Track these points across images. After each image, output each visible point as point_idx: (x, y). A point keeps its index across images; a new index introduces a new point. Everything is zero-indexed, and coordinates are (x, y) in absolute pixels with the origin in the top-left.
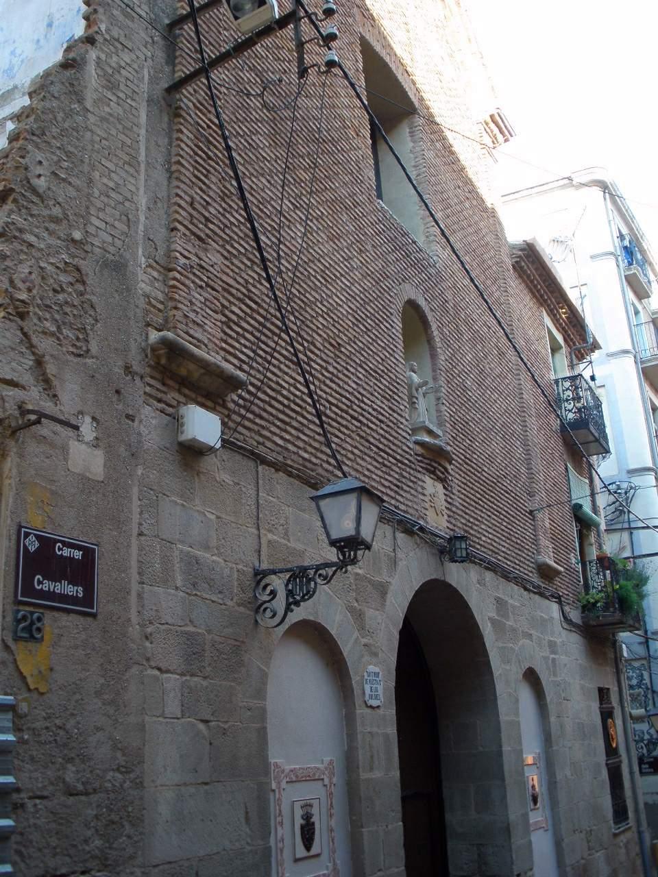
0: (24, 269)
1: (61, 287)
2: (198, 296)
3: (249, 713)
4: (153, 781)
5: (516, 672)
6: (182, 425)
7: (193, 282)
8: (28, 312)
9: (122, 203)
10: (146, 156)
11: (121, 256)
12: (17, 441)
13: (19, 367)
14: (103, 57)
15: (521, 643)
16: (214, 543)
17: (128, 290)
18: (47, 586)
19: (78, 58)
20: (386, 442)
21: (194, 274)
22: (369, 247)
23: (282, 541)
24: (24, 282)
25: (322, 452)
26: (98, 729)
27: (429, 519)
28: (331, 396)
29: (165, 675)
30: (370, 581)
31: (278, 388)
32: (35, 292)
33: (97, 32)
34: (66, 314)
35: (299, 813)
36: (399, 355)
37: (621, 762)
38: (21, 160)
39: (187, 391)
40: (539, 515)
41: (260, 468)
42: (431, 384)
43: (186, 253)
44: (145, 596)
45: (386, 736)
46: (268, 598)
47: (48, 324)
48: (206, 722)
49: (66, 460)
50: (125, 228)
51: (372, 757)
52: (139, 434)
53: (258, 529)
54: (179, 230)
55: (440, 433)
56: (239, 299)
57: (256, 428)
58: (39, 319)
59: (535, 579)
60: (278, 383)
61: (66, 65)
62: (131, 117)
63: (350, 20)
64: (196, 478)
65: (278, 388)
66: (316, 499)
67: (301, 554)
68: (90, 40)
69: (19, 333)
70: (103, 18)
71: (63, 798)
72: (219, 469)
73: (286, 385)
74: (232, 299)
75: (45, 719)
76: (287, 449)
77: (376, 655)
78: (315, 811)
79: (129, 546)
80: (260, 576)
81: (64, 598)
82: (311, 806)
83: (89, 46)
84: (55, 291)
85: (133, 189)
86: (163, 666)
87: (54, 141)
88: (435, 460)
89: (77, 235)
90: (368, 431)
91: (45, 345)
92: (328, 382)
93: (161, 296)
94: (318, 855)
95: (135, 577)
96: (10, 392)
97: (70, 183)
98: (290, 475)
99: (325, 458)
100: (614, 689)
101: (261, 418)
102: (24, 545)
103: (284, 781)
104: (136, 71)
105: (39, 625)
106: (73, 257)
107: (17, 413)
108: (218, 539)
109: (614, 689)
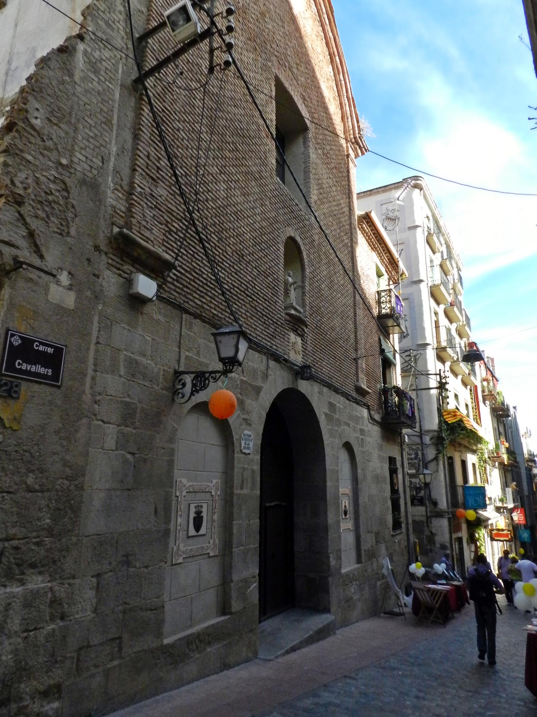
0: (22, 176)
1: (51, 191)
2: (149, 213)
3: (163, 451)
4: (91, 486)
5: (338, 442)
6: (132, 284)
7: (146, 204)
8: (24, 203)
9: (99, 148)
10: (118, 121)
11: (96, 180)
12: (10, 279)
13: (18, 236)
14: (89, 50)
15: (342, 428)
16: (149, 353)
17: (100, 201)
18: (24, 367)
19: (70, 47)
20: (267, 311)
21: (147, 199)
22: (268, 203)
23: (196, 357)
24: (21, 183)
25: (226, 312)
26: (55, 454)
27: (291, 356)
28: (235, 282)
29: (106, 425)
30: (250, 384)
31: (201, 273)
32: (30, 191)
33: (85, 32)
34: (53, 208)
35: (193, 510)
36: (281, 266)
37: (399, 498)
38: (23, 106)
39: (137, 266)
40: (359, 361)
41: (184, 315)
42: (300, 284)
43: (142, 185)
44: (98, 378)
45: (253, 471)
46: (180, 387)
47: (39, 212)
48: (133, 454)
49: (46, 294)
50: (101, 164)
51: (243, 481)
52: (101, 286)
53: (179, 348)
54: (137, 171)
55: (302, 311)
56: (178, 219)
57: (183, 293)
58: (33, 208)
59: (354, 394)
60: (200, 270)
61: (61, 50)
62: (108, 93)
63: (270, 64)
64: (140, 317)
65: (201, 273)
66: (214, 335)
67: (207, 365)
68: (80, 37)
69: (17, 214)
70: (91, 24)
71: (23, 494)
72: (154, 311)
73: (206, 273)
74: (173, 218)
75: (15, 445)
76: (203, 308)
77: (250, 425)
78: (204, 510)
79: (88, 349)
80: (178, 374)
81: (36, 375)
82: (202, 507)
83: (79, 41)
84: (46, 193)
85: (107, 140)
86: (105, 419)
87: (49, 98)
88: (297, 324)
89: (64, 161)
90: (257, 304)
91: (34, 224)
92: (233, 274)
93: (123, 209)
94: (204, 535)
95: (91, 367)
96: (7, 250)
97: (60, 127)
98: (204, 321)
99: (227, 315)
100: (398, 459)
101: (188, 288)
102: (10, 341)
103: (185, 492)
104: (113, 65)
105: (16, 389)
106: (61, 174)
107: (11, 262)
108: (152, 352)
109: (398, 459)
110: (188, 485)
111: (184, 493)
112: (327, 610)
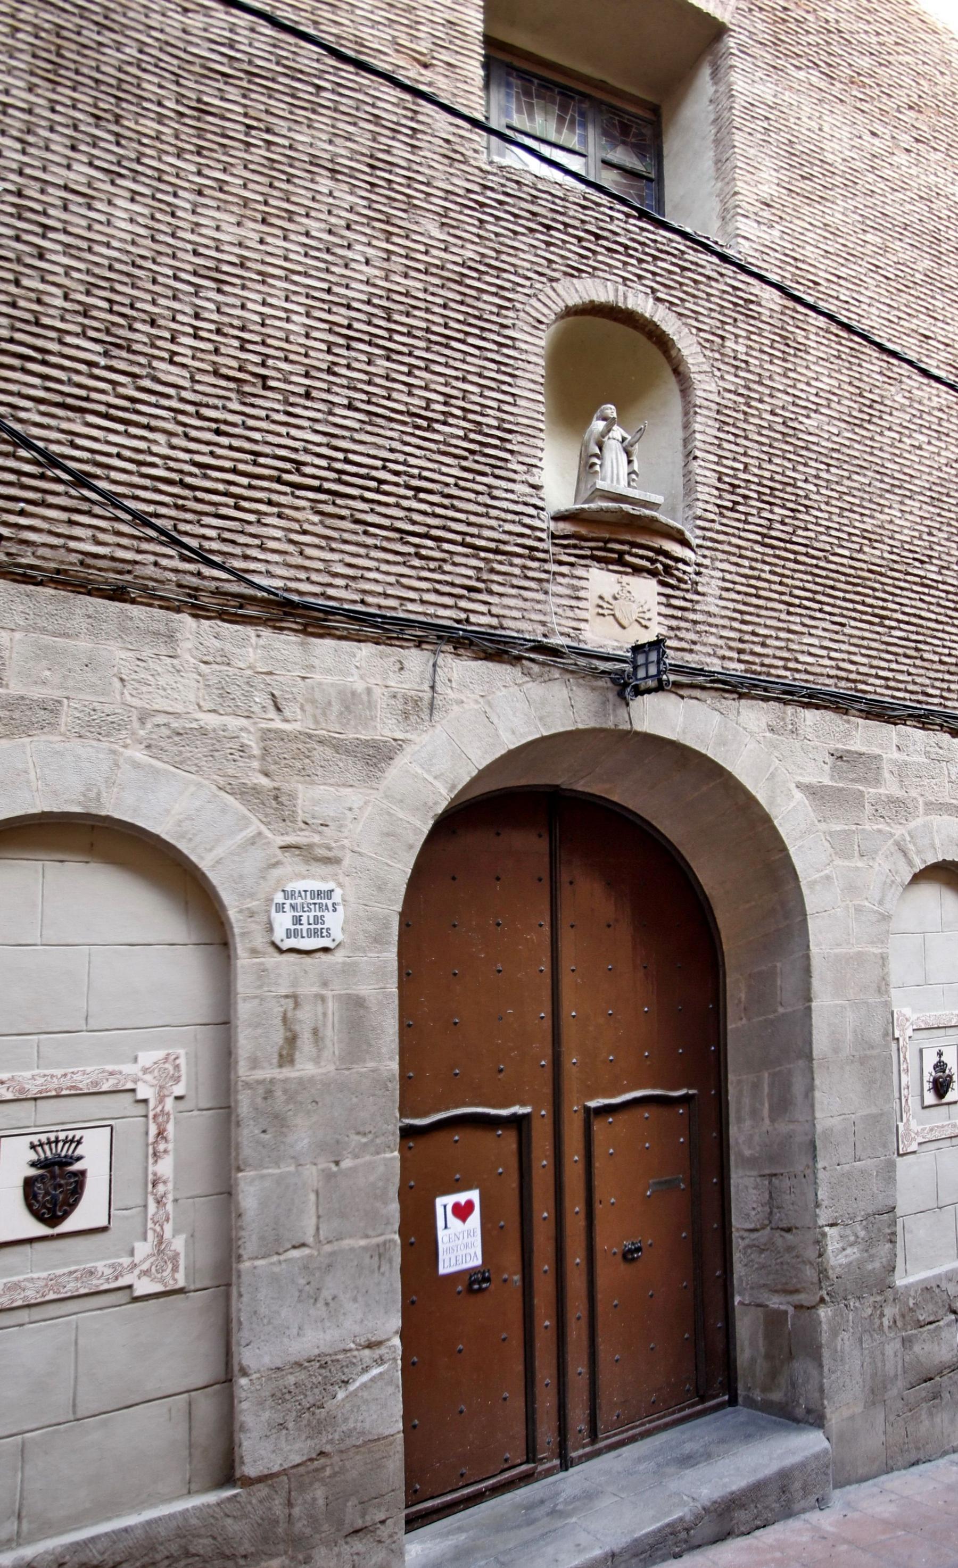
110: (913, 1017)
111: (909, 1032)
112: (814, 1419)
